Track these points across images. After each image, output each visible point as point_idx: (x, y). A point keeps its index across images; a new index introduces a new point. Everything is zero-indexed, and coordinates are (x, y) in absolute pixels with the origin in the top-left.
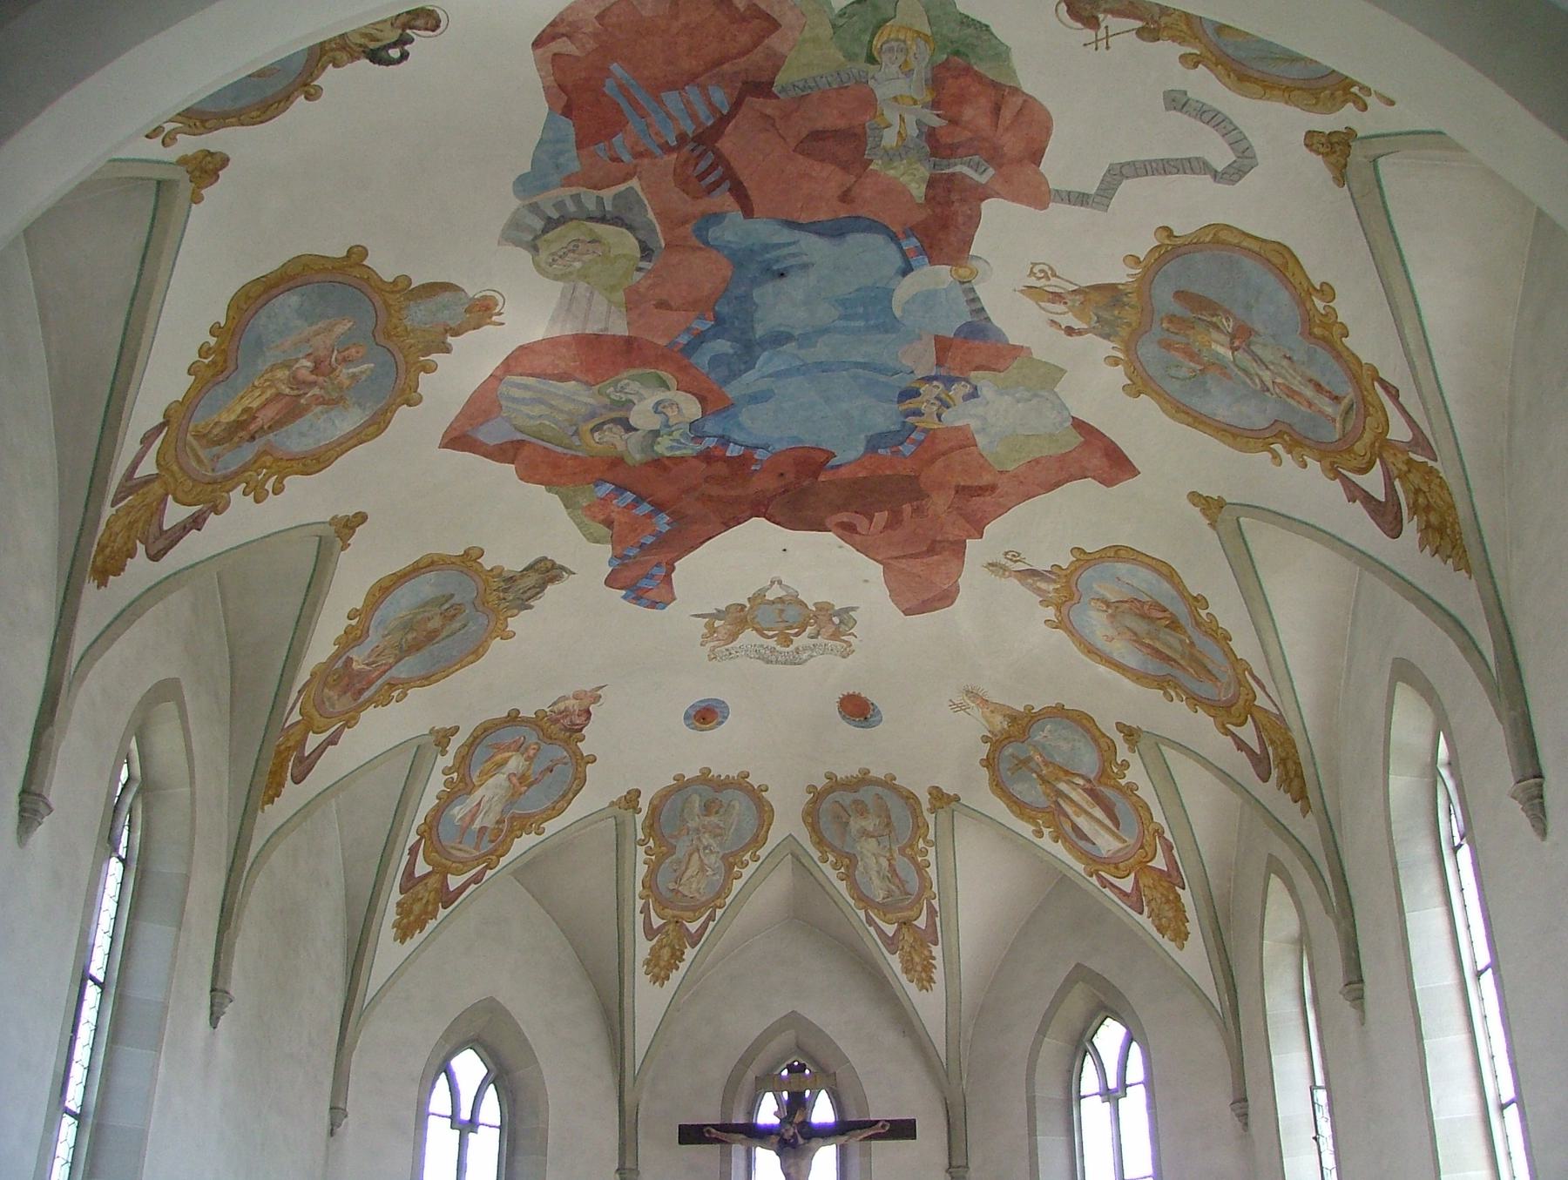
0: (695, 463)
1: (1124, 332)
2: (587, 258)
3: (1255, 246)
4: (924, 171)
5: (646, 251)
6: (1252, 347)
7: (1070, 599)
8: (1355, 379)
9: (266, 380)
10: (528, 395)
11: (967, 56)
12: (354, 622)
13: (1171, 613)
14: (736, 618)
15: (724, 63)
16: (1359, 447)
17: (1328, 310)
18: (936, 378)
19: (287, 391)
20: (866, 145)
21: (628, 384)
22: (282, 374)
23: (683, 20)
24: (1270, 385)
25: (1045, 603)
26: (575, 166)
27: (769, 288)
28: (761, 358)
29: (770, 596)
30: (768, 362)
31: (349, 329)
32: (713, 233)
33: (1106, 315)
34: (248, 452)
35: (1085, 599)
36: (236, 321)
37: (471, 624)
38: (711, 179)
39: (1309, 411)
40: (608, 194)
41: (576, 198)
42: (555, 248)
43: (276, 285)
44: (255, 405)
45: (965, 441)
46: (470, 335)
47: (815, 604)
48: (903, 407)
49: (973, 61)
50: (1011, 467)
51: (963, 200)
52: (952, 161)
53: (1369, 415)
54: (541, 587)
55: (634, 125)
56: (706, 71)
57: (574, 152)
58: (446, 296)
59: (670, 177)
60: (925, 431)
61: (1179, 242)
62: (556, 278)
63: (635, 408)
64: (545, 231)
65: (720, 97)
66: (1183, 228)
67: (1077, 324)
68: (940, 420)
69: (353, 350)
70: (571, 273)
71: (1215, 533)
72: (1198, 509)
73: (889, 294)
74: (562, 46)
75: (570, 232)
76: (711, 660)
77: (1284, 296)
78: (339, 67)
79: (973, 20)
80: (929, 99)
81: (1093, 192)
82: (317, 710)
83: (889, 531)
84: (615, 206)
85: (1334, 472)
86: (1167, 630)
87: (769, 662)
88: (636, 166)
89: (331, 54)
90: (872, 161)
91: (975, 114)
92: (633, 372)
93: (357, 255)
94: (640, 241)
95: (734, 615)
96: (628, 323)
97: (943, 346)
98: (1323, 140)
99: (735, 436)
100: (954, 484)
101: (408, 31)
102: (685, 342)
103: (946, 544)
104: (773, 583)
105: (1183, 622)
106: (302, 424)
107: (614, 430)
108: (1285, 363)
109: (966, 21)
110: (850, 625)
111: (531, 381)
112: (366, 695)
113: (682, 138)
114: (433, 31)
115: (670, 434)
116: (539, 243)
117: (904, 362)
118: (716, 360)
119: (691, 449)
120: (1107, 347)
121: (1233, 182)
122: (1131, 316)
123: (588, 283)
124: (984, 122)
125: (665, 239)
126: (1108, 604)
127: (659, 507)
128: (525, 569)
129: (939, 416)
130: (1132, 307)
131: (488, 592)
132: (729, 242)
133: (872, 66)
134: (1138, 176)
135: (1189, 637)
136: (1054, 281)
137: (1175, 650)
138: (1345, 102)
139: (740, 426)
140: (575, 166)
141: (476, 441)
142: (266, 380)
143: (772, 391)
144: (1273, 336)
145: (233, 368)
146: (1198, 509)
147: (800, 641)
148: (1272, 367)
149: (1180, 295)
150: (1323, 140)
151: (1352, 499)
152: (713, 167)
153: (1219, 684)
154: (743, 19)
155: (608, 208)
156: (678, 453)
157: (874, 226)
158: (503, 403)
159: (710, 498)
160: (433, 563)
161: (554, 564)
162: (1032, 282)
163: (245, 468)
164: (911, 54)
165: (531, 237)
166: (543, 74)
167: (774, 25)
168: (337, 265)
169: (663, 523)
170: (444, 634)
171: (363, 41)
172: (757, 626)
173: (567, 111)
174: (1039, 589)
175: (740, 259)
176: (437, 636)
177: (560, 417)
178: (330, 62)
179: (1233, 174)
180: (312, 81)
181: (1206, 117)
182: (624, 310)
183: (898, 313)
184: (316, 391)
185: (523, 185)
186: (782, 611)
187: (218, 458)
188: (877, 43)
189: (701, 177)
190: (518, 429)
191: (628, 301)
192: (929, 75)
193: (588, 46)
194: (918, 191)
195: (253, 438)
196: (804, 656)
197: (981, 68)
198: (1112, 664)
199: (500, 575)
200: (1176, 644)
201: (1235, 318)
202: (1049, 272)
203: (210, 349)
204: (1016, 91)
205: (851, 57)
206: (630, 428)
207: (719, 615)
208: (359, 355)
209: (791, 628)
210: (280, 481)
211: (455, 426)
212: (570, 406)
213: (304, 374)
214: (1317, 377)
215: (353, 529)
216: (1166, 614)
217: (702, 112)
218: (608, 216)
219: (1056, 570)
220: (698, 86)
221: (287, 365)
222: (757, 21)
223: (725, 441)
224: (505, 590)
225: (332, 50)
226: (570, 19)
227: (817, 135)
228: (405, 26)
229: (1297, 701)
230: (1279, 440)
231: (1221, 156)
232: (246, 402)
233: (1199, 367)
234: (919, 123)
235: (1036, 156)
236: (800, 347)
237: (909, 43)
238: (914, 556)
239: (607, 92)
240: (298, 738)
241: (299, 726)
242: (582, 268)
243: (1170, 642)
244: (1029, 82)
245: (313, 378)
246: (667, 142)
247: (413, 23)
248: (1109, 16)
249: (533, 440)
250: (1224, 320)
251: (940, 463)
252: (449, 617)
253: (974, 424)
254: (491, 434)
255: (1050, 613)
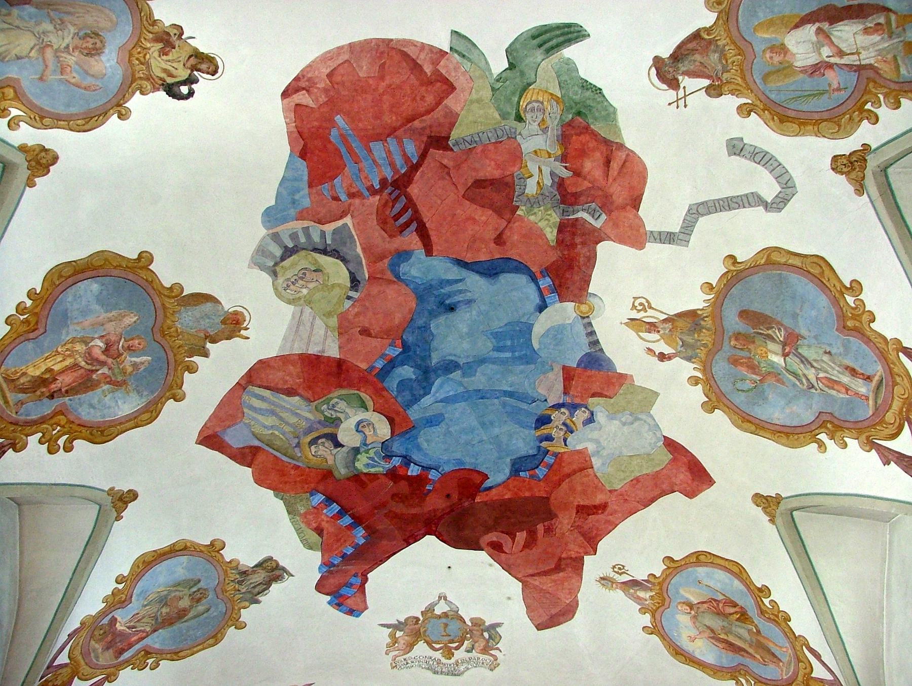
0: (383, 479)
1: (702, 353)
2: (311, 285)
3: (797, 262)
4: (555, 218)
5: (355, 282)
6: (800, 351)
7: (663, 605)
8: (883, 356)
9: (67, 350)
10: (263, 405)
11: (586, 116)
12: (121, 586)
13: (742, 607)
14: (412, 629)
15: (414, 120)
16: (890, 417)
17: (857, 303)
18: (562, 405)
19: (83, 364)
20: (514, 191)
21: (337, 403)
22: (81, 348)
23: (387, 81)
24: (814, 381)
25: (643, 611)
26: (306, 203)
27: (442, 319)
28: (436, 383)
29: (438, 611)
30: (442, 387)
31: (135, 322)
32: (404, 268)
33: (689, 339)
34: (47, 407)
35: (673, 604)
36: (49, 292)
37: (212, 609)
38: (402, 220)
39: (847, 396)
40: (329, 228)
41: (306, 230)
42: (289, 274)
43: (83, 271)
44: (57, 368)
45: (583, 463)
46: (224, 343)
47: (471, 620)
48: (539, 433)
49: (590, 121)
50: (618, 486)
51: (584, 244)
52: (576, 207)
53: (897, 384)
54: (267, 584)
55: (350, 168)
56: (403, 125)
57: (306, 191)
58: (209, 305)
59: (374, 217)
60: (556, 455)
61: (742, 267)
62: (289, 302)
63: (342, 426)
64: (283, 259)
65: (412, 149)
66: (744, 255)
67: (668, 350)
68: (566, 445)
69: (137, 342)
70: (300, 298)
71: (774, 526)
72: (760, 508)
73: (530, 327)
74: (302, 98)
75: (300, 261)
76: (393, 668)
77: (823, 301)
78: (224, 542)
79: (591, 84)
80: (560, 153)
81: (677, 231)
82: (84, 659)
83: (527, 550)
84: (333, 240)
85: (870, 445)
86: (737, 623)
87: (436, 672)
88: (350, 205)
89: (139, 82)
90: (518, 207)
91: (591, 166)
92: (343, 392)
93: (145, 259)
94: (350, 272)
95: (411, 627)
96: (340, 348)
97: (568, 375)
98: (845, 162)
99: (416, 457)
100: (576, 504)
101: (195, 73)
102: (380, 367)
103: (569, 561)
104: (440, 598)
105: (750, 614)
106: (93, 396)
107: (326, 445)
108: (826, 358)
109: (586, 85)
110: (497, 641)
111: (267, 393)
112: (126, 655)
113: (384, 182)
114: (213, 75)
115: (367, 452)
116: (278, 269)
117: (539, 391)
118: (403, 384)
119: (382, 467)
120: (688, 369)
121: (780, 210)
122: (706, 338)
123: (311, 308)
124: (598, 174)
125: (368, 272)
126: (691, 606)
127: (358, 520)
128: (256, 566)
129: (565, 440)
130: (708, 330)
131: (227, 581)
132: (415, 277)
133: (519, 124)
134: (711, 213)
135: (756, 626)
136: (650, 312)
137: (745, 641)
138: (861, 120)
139: (419, 448)
140: (306, 203)
141: (223, 441)
142: (67, 350)
143: (442, 415)
144: (816, 337)
145: (42, 330)
146: (760, 508)
147: (460, 654)
148: (815, 364)
149: (744, 314)
150: (845, 162)
151: (886, 463)
152: (404, 210)
153: (781, 664)
154: (430, 83)
155: (329, 242)
156: (373, 470)
157: (520, 268)
158: (245, 410)
159: (396, 516)
160: (185, 548)
161: (278, 565)
162: (635, 315)
163: (43, 420)
164: (547, 114)
165: (273, 263)
166: (288, 120)
167: (450, 88)
168: (130, 265)
169: (360, 535)
170: (191, 615)
171: (163, 75)
172: (428, 639)
173: (303, 155)
174: (639, 598)
175: (423, 293)
176: (186, 615)
177: (287, 429)
178: (137, 89)
179: (778, 204)
180: (124, 104)
181: (758, 159)
182: (336, 334)
183: (536, 345)
184: (105, 370)
185: (271, 216)
186: (446, 625)
187: (22, 404)
188: (523, 104)
189: (396, 218)
190: (255, 436)
191: (340, 327)
192: (560, 133)
193: (320, 99)
194: (551, 234)
195: (52, 397)
196: (462, 668)
197: (596, 127)
198: (693, 662)
199: (236, 568)
200: (746, 635)
201: (785, 329)
202: (646, 304)
203: (25, 308)
204: (621, 146)
205: (504, 116)
206: (338, 445)
207: (398, 626)
208: (141, 347)
209: (452, 642)
210: (70, 441)
211: (208, 425)
212: (293, 420)
213: (97, 353)
214: (851, 364)
215: (126, 504)
216: (737, 609)
217: (399, 161)
218: (328, 249)
219: (652, 580)
220: (396, 137)
221: (85, 341)
222: (439, 84)
223: (407, 461)
224: (240, 583)
225: (141, 78)
226: (309, 75)
227: (479, 184)
228: (194, 68)
229: (850, 661)
230: (823, 430)
231: (769, 189)
232: (49, 364)
233: (758, 378)
234: (552, 174)
235: (636, 202)
236: (464, 375)
237: (545, 103)
238: (545, 573)
239: (332, 140)
240: (65, 679)
241: (64, 670)
242: (308, 293)
243: (741, 634)
244: (631, 138)
245: (103, 358)
246: (372, 185)
247: (199, 66)
248: (686, 77)
249: (267, 448)
250: (777, 331)
251: (565, 485)
252: (197, 599)
253: (591, 447)
254: (236, 438)
255: (646, 620)
